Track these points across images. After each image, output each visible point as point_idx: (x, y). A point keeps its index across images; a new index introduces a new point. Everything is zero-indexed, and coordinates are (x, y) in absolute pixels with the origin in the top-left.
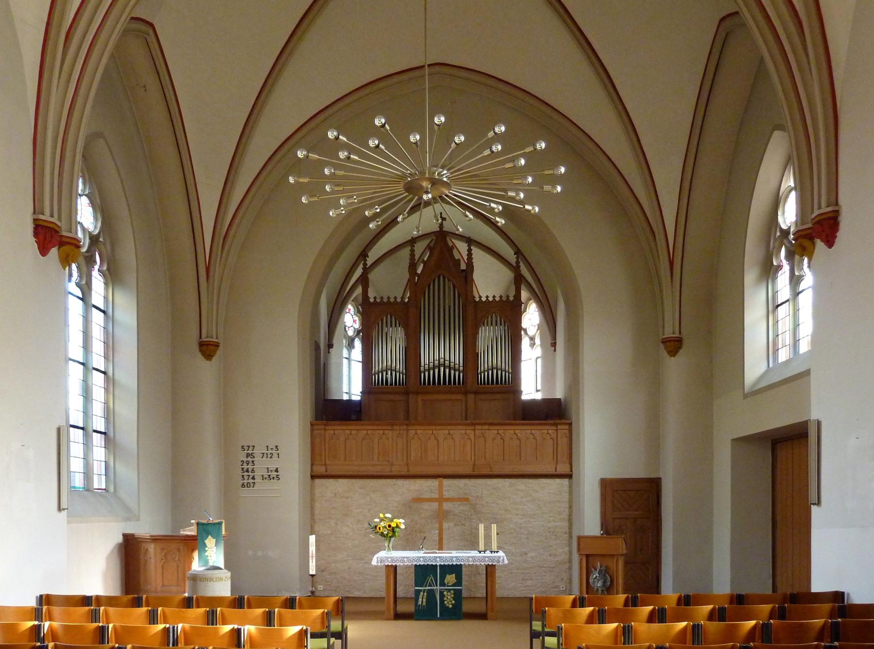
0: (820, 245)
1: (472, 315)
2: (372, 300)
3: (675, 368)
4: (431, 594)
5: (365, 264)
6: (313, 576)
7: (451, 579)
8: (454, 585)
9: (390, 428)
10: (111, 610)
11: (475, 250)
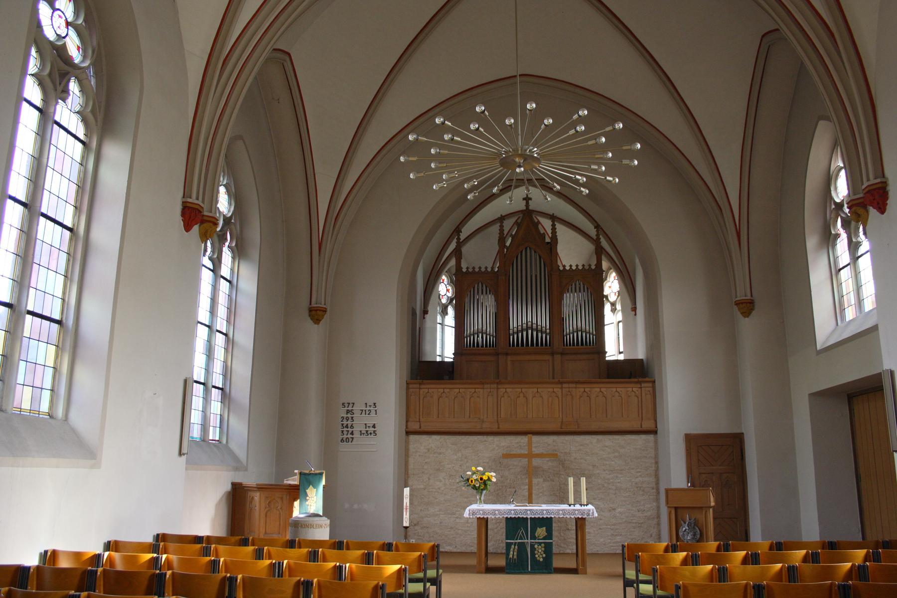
0: (873, 212)
1: (556, 283)
2: (464, 270)
3: (749, 328)
4: (522, 547)
5: (459, 239)
6: (406, 528)
7: (541, 532)
8: (544, 538)
9: (481, 386)
10: (221, 548)
11: (559, 226)
